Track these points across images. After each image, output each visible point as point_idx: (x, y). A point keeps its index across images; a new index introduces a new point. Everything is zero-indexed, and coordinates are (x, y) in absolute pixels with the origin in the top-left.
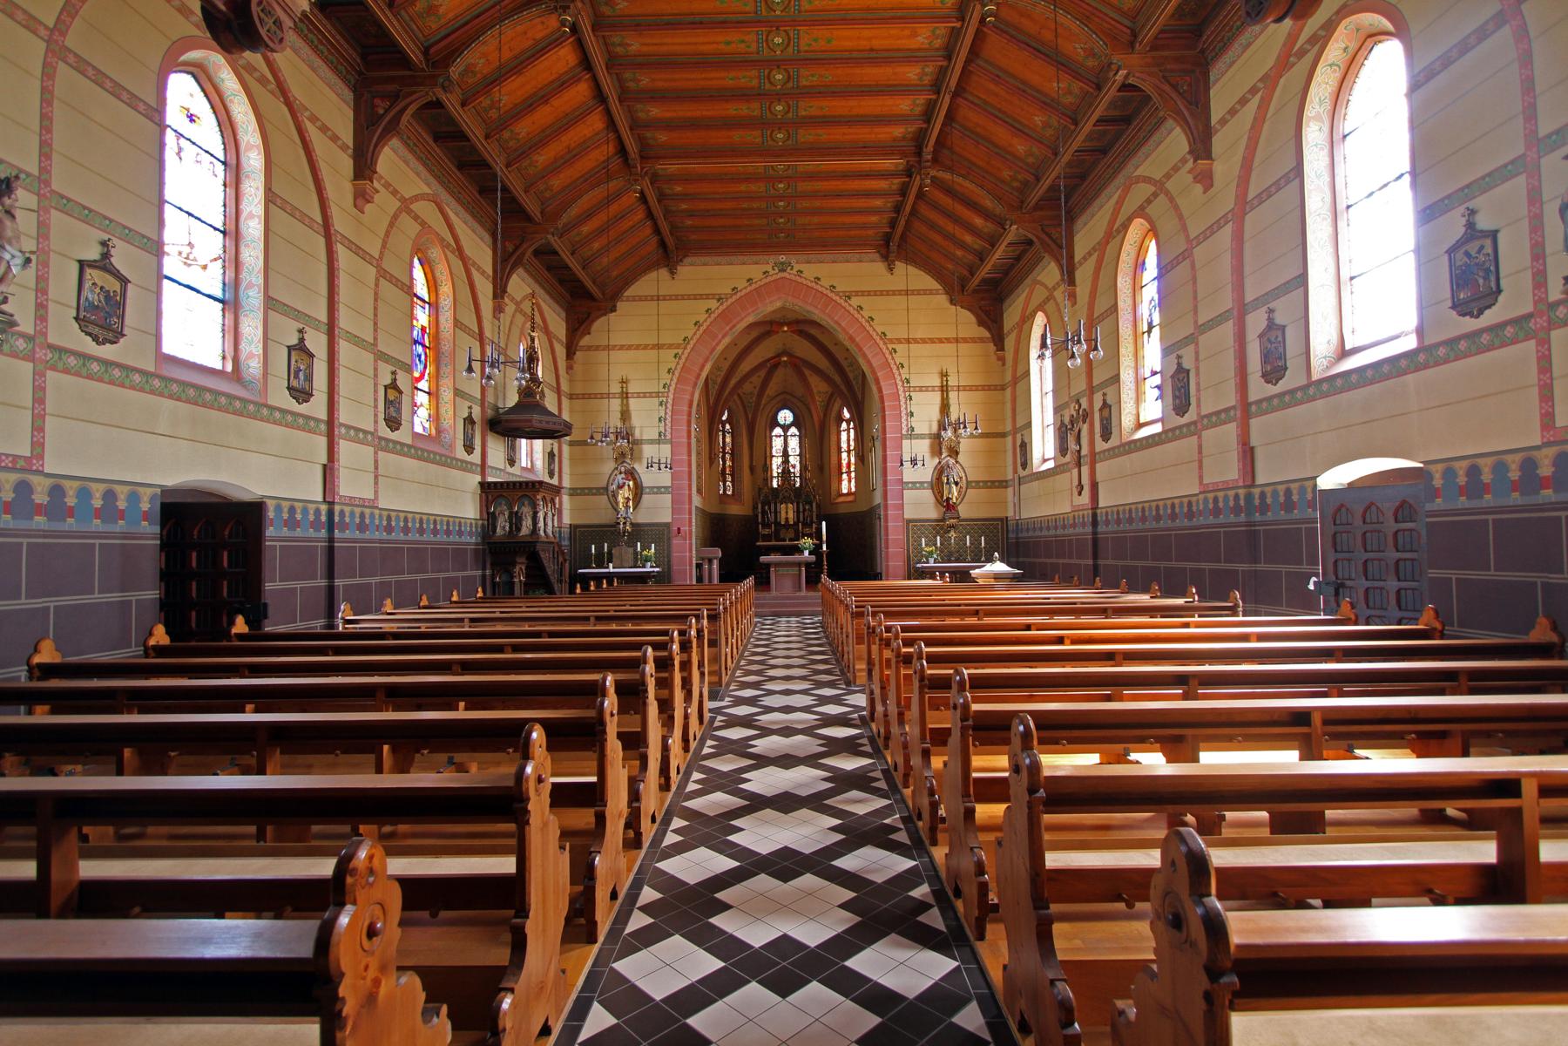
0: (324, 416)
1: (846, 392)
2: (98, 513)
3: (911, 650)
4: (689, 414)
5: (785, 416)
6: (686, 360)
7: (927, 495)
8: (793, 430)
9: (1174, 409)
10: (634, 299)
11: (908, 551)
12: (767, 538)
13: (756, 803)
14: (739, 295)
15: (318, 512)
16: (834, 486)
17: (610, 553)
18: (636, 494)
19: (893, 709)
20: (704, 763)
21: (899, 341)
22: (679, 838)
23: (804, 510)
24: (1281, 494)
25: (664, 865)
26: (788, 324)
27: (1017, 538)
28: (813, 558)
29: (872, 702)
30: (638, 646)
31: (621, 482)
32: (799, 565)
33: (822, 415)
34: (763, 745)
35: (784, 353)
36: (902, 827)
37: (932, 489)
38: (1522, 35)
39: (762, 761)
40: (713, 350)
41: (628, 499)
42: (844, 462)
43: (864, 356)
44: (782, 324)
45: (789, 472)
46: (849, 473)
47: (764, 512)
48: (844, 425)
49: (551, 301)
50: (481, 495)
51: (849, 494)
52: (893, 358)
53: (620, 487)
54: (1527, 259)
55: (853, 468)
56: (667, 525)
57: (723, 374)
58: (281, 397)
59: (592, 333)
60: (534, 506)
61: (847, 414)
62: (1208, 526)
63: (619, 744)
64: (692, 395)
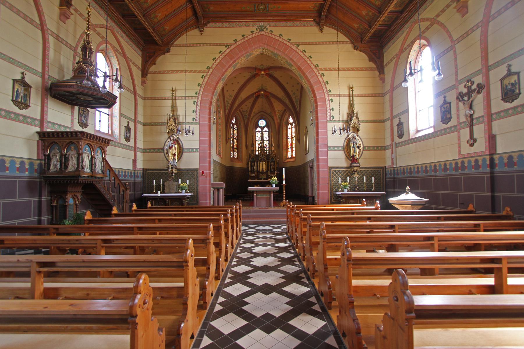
0: (133, 145)
1: (293, 110)
2: (18, 169)
4: (210, 109)
5: (262, 123)
6: (209, 78)
7: (341, 154)
8: (266, 129)
9: (442, 121)
10: (180, 45)
11: (330, 184)
12: (253, 178)
13: (256, 269)
14: (237, 44)
15: (131, 173)
16: (285, 154)
17: (163, 185)
18: (180, 152)
20: (237, 255)
21: (326, 69)
23: (271, 165)
24: (424, 167)
25: (226, 289)
26: (264, 70)
27: (394, 178)
30: (218, 215)
31: (171, 145)
32: (270, 192)
33: (279, 122)
34: (257, 250)
35: (262, 90)
36: (304, 276)
37: (344, 150)
38: (455, 54)
39: (257, 255)
41: (175, 155)
42: (289, 143)
43: (306, 78)
44: (261, 70)
47: (252, 166)
48: (290, 126)
49: (125, 37)
50: (38, 142)
51: (292, 158)
52: (322, 79)
53: (171, 148)
54: (456, 112)
55: (294, 146)
56: (196, 169)
57: (232, 98)
58: (123, 141)
59: (157, 64)
60: (78, 149)
61: (291, 120)
62: (472, 174)
63: (214, 246)
64: (212, 98)
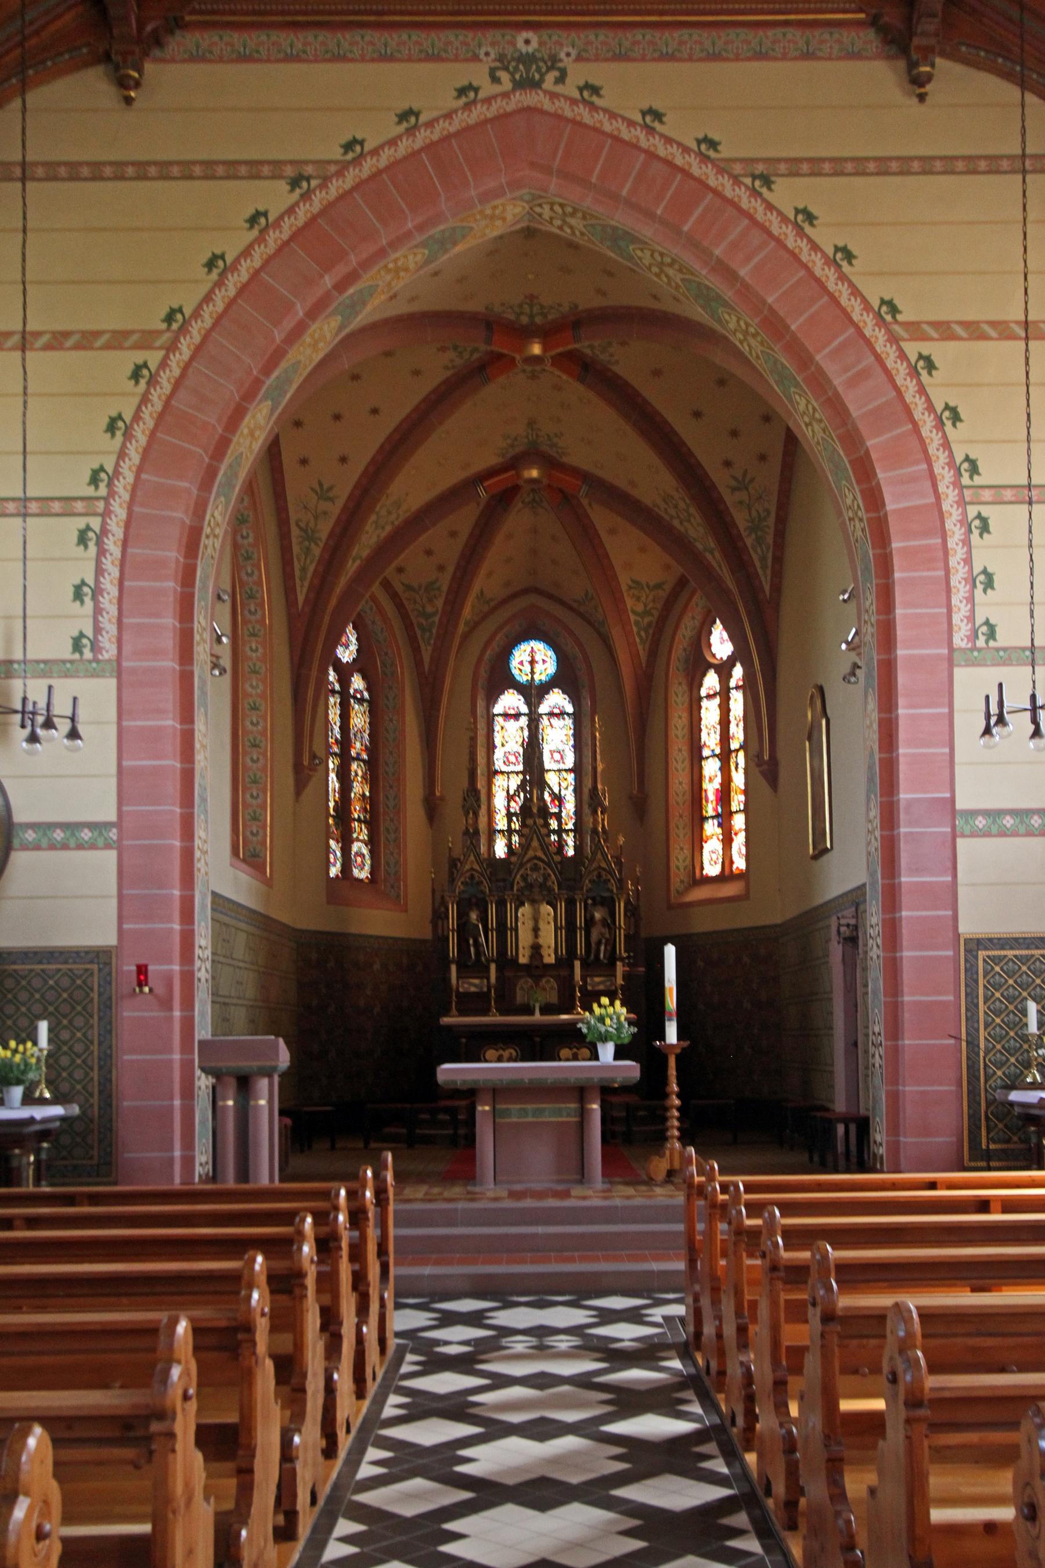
1: (730, 583)
3: (806, 1255)
4: (188, 577)
6: (177, 384)
8: (557, 699)
11: (972, 1044)
14: (368, 166)
16: (679, 858)
19: (730, 1330)
22: (350, 1550)
23: (590, 922)
26: (547, 333)
28: (631, 1069)
29: (697, 1314)
32: (580, 1092)
33: (643, 656)
35: (532, 454)
40: (276, 357)
42: (711, 787)
43: (819, 382)
44: (524, 333)
45: (544, 813)
46: (725, 818)
47: (464, 930)
48: (711, 681)
51: (727, 876)
52: (922, 390)
55: (738, 801)
56: (100, 956)
64: (200, 510)
